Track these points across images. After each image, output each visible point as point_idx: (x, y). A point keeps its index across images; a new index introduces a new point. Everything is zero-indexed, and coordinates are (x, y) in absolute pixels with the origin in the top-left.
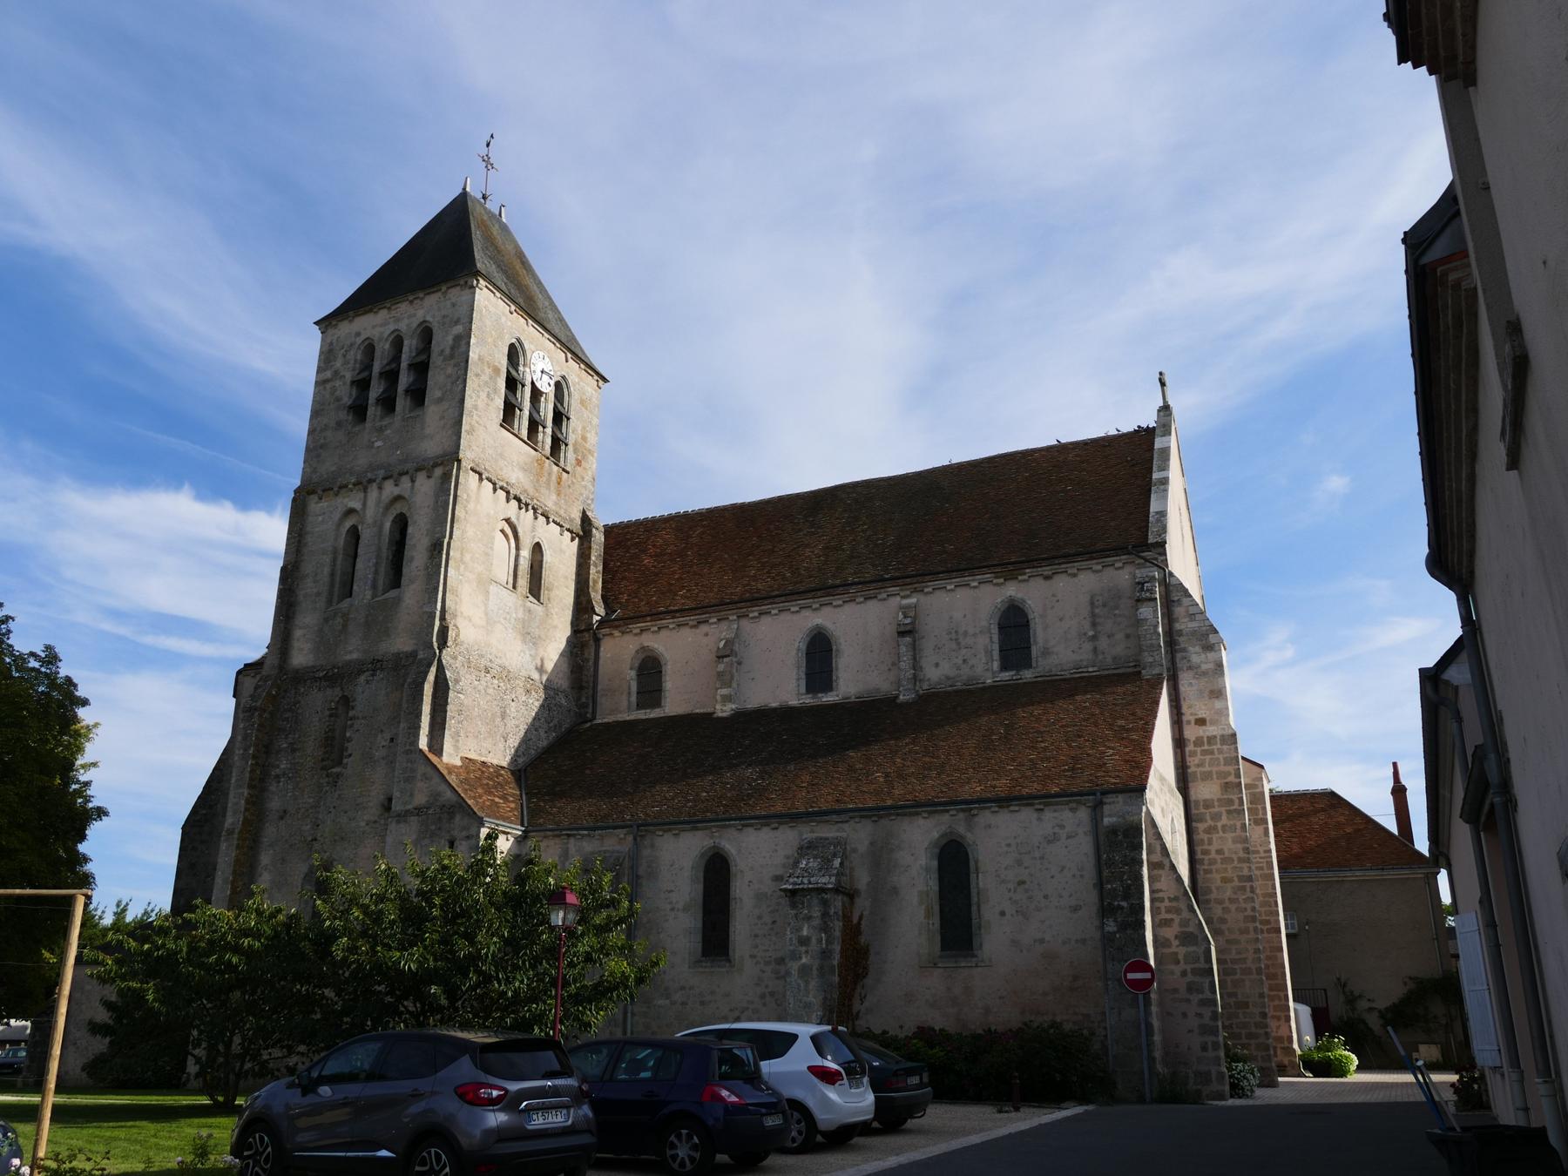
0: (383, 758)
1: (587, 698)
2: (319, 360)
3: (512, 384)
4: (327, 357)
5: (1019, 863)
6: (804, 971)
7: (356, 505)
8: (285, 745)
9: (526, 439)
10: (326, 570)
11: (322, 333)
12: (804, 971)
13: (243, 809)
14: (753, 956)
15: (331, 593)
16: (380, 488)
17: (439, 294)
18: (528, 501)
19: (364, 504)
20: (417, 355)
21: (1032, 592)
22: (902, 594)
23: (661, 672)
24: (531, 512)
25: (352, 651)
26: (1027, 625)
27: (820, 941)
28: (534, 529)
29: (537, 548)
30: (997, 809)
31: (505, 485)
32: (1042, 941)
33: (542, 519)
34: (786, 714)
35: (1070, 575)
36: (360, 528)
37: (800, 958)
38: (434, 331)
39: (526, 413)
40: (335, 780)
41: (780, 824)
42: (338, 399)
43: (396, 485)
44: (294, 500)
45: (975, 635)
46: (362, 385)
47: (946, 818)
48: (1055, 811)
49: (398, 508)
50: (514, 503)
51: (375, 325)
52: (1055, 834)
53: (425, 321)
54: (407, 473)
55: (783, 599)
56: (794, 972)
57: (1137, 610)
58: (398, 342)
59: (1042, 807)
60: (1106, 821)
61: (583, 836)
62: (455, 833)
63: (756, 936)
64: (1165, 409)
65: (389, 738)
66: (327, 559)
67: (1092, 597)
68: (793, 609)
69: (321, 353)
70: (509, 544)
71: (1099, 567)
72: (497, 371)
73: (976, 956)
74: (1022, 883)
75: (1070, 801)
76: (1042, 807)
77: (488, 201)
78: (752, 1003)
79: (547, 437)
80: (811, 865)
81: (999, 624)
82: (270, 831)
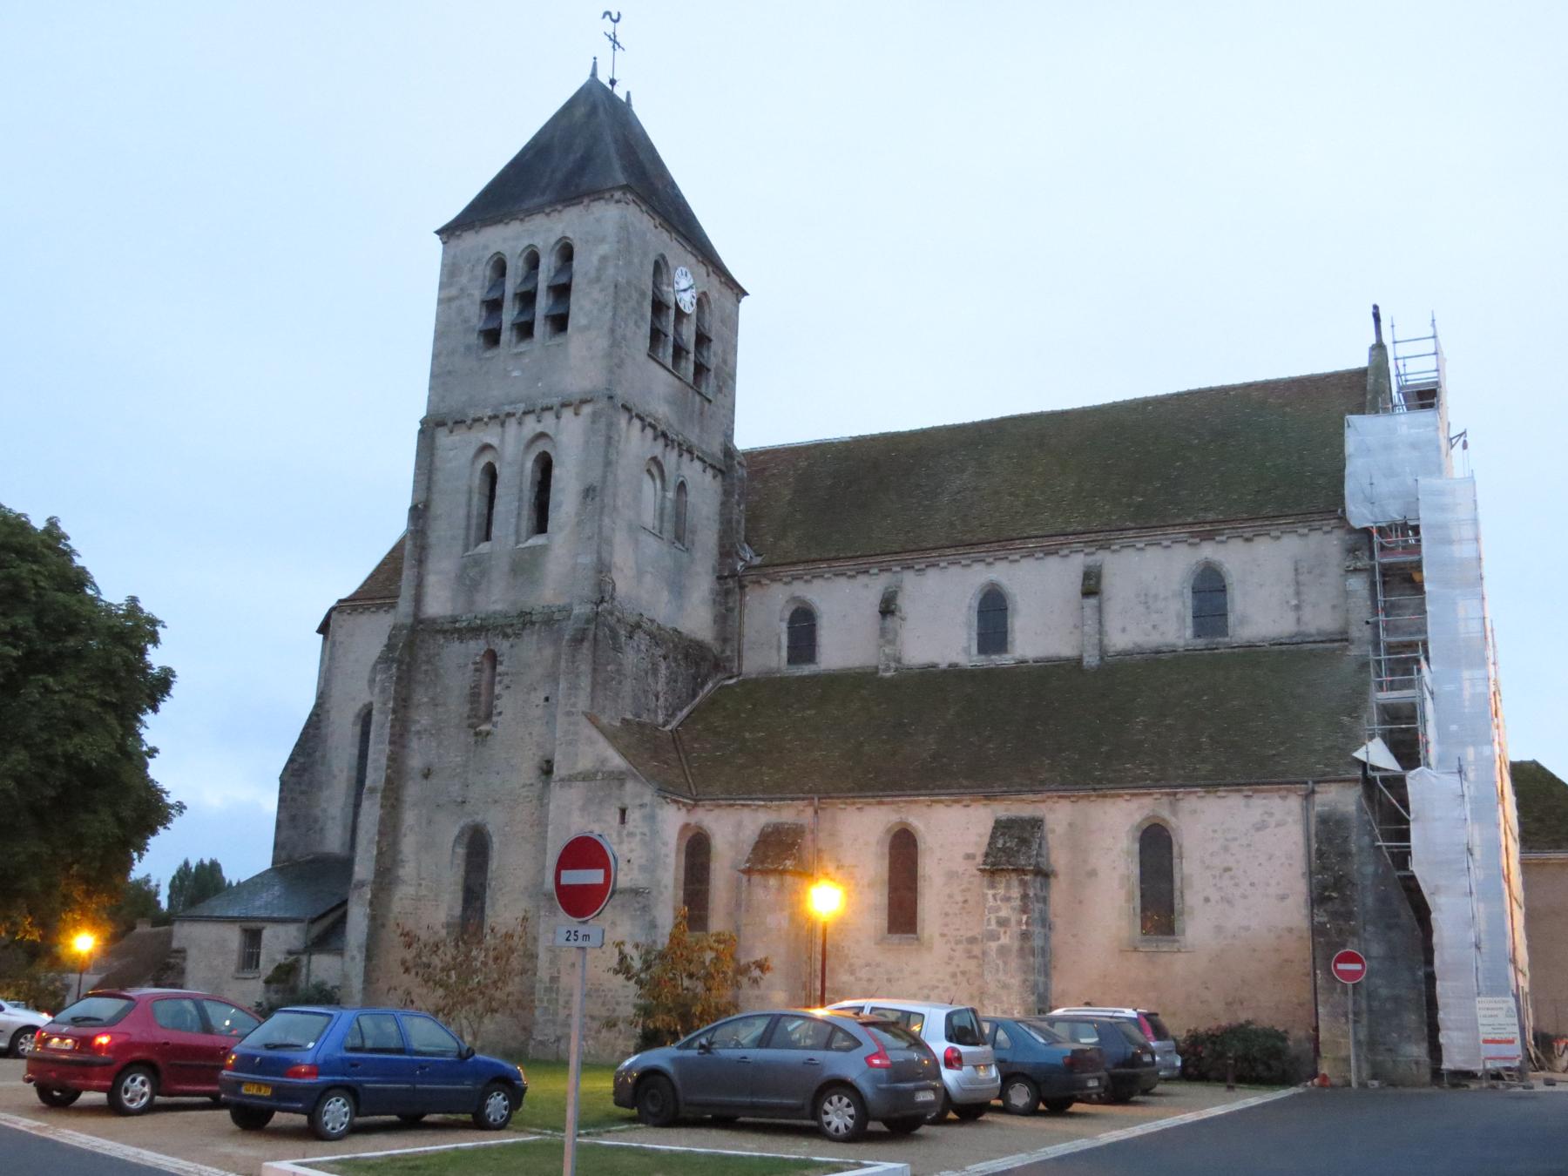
0: (538, 719)
1: (732, 651)
2: (441, 275)
3: (659, 306)
4: (450, 273)
5: (1226, 849)
6: (1003, 951)
7: (494, 441)
8: (425, 700)
9: (671, 368)
10: (462, 512)
11: (444, 243)
12: (1003, 951)
13: (385, 767)
14: (943, 935)
15: (467, 537)
16: (520, 423)
17: (581, 207)
18: (675, 437)
19: (502, 440)
20: (555, 276)
21: (1231, 556)
22: (1087, 550)
23: (815, 625)
24: (676, 450)
25: (496, 599)
26: (1223, 590)
27: (1019, 922)
28: (679, 467)
29: (682, 487)
30: (1202, 794)
31: (653, 422)
32: (1247, 929)
33: (686, 456)
34: (955, 674)
35: (1272, 538)
36: (497, 466)
37: (999, 939)
38: (575, 250)
39: (671, 338)
40: (482, 738)
41: (973, 801)
42: (466, 321)
43: (539, 421)
44: (421, 432)
45: (1166, 599)
46: (493, 306)
47: (1147, 801)
48: (1264, 798)
49: (541, 446)
50: (661, 442)
51: (508, 239)
52: (1264, 821)
53: (565, 238)
54: (551, 408)
55: (953, 551)
56: (993, 954)
57: (1346, 580)
58: (533, 261)
59: (1250, 793)
60: (1318, 808)
61: (760, 806)
62: (627, 801)
63: (947, 914)
64: (1379, 348)
65: (543, 697)
66: (463, 499)
67: (1296, 562)
68: (963, 562)
69: (444, 265)
70: (655, 484)
71: (1306, 531)
72: (643, 294)
73: (1178, 941)
74: (1227, 869)
75: (1280, 789)
76: (1250, 793)
77: (615, 87)
78: (943, 981)
79: (688, 367)
80: (1008, 845)
81: (1193, 588)
82: (413, 791)
